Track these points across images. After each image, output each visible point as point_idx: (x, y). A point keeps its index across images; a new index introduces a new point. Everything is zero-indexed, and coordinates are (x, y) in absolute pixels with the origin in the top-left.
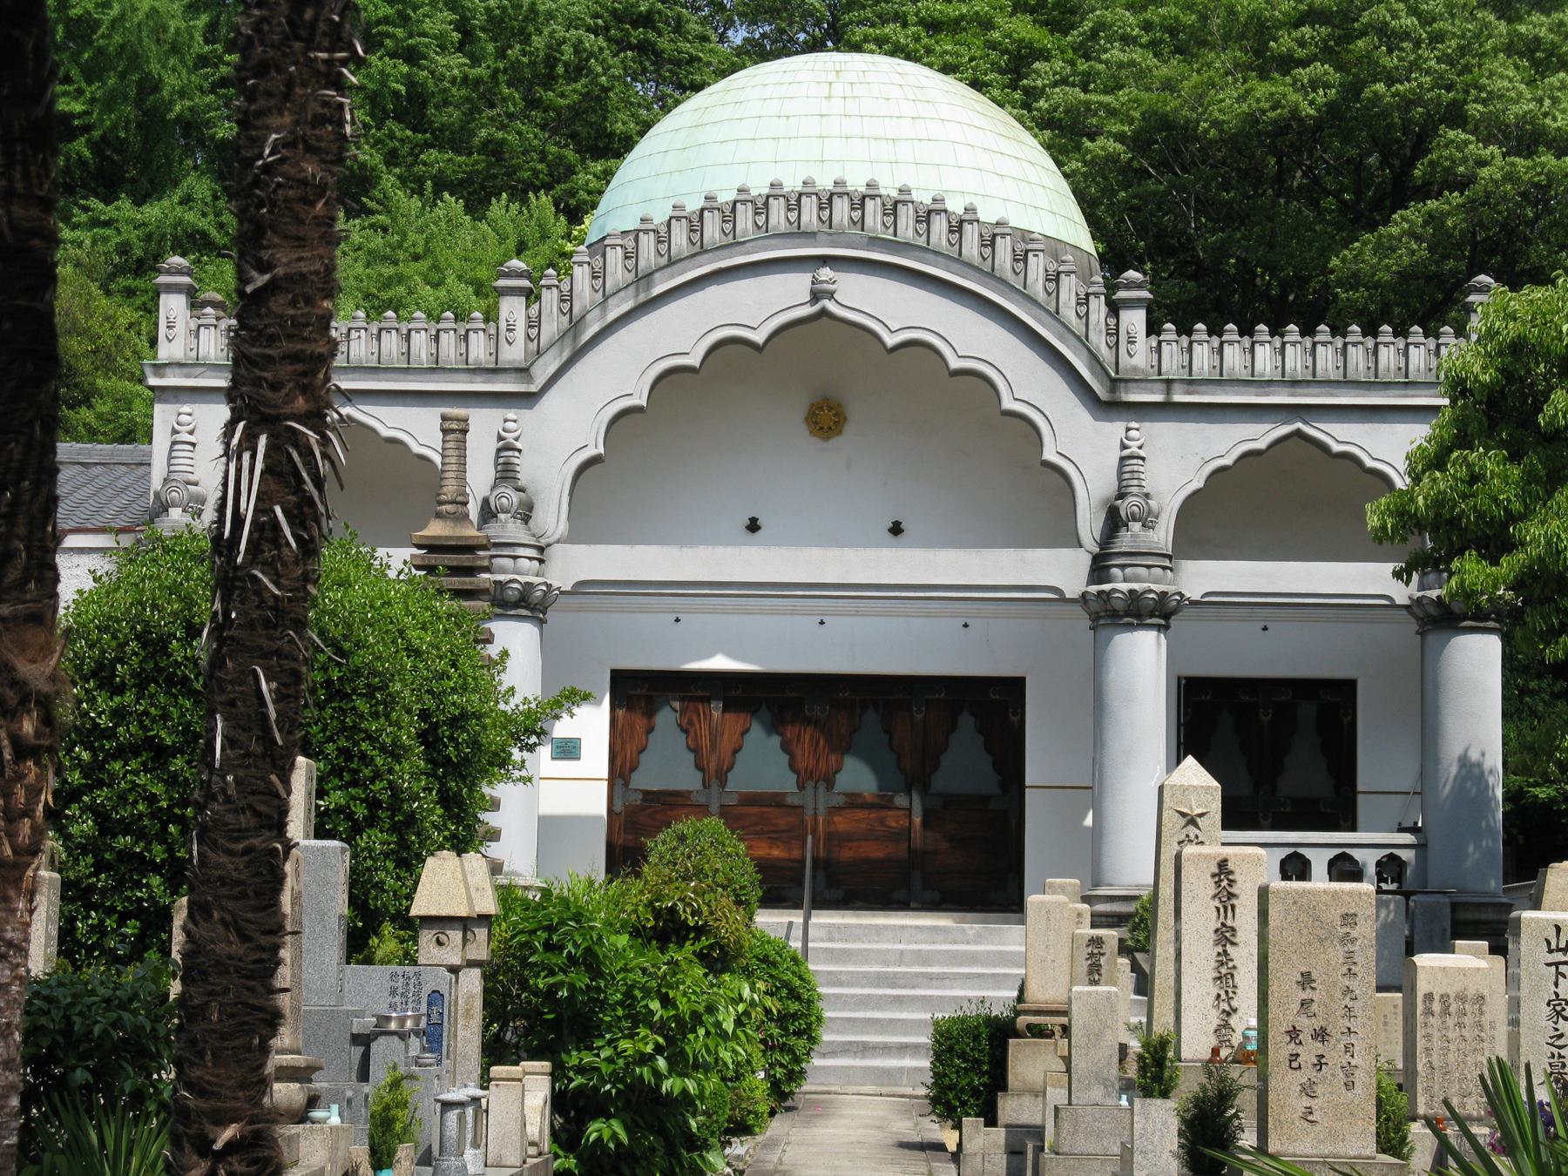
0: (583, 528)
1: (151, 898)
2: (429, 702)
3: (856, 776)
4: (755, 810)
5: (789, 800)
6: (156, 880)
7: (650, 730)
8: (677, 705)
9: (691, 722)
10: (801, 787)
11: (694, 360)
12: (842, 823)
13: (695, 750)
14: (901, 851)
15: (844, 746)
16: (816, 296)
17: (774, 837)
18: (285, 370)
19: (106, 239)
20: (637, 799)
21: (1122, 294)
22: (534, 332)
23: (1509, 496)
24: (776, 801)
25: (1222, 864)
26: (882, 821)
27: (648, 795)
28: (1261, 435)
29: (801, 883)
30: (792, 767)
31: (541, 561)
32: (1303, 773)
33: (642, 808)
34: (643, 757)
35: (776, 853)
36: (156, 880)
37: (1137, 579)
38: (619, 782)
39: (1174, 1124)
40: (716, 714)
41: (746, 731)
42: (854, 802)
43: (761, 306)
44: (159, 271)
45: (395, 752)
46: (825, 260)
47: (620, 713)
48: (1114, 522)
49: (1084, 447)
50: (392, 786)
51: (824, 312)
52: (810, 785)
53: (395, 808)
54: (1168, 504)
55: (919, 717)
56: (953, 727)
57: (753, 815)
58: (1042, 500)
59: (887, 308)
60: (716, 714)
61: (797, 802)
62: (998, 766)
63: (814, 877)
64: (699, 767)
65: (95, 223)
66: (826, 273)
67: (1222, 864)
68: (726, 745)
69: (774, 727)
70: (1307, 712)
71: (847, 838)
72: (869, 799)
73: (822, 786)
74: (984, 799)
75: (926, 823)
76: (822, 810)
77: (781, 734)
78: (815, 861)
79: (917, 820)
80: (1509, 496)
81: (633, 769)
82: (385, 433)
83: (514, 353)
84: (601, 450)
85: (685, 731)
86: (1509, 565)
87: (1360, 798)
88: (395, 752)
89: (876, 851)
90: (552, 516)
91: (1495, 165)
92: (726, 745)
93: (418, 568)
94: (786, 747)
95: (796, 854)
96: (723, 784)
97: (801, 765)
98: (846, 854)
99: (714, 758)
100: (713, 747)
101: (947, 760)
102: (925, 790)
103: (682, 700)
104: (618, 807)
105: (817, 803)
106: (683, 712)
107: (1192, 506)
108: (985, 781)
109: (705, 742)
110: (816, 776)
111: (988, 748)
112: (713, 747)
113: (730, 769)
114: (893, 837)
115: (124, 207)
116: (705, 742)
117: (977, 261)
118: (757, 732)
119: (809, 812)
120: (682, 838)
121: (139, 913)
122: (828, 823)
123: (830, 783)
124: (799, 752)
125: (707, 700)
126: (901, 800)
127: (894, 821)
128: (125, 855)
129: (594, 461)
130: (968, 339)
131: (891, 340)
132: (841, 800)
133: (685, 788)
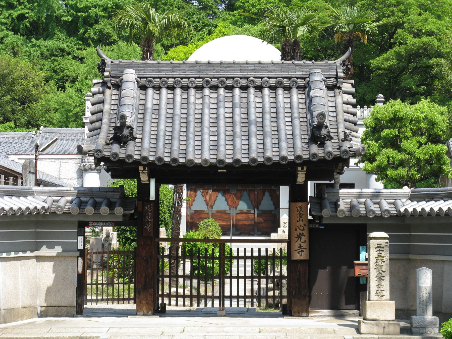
1: (127, 236)
2: (168, 204)
3: (243, 206)
4: (220, 214)
5: (227, 212)
6: (128, 233)
7: (195, 196)
8: (201, 191)
9: (205, 195)
10: (230, 209)
12: (239, 217)
13: (206, 201)
14: (253, 223)
15: (240, 199)
17: (224, 220)
18: (179, 188)
19: (37, 50)
20: (193, 212)
23: (376, 150)
24: (224, 212)
25: (283, 230)
26: (248, 216)
27: (195, 211)
29: (230, 231)
30: (228, 204)
33: (194, 214)
34: (194, 203)
35: (224, 224)
36: (128, 233)
38: (189, 208)
40: (210, 193)
41: (217, 197)
42: (242, 212)
44: (85, 96)
45: (165, 213)
47: (189, 192)
50: (164, 218)
52: (232, 208)
53: (165, 222)
55: (256, 193)
56: (264, 195)
57: (219, 215)
60: (210, 193)
61: (229, 212)
62: (274, 204)
63: (233, 229)
64: (207, 205)
65: (34, 46)
67: (283, 230)
68: (213, 200)
69: (223, 195)
71: (240, 220)
72: (245, 212)
73: (234, 208)
74: (271, 211)
75: (258, 216)
76: (234, 214)
77: (225, 197)
78: (233, 225)
79: (256, 216)
80: (376, 150)
81: (192, 205)
85: (203, 197)
86: (375, 164)
88: (165, 213)
89: (246, 223)
91: (411, 40)
92: (213, 200)
94: (226, 200)
95: (229, 224)
96: (212, 208)
97: (230, 204)
98: (240, 223)
99: (210, 202)
100: (210, 200)
101: (263, 202)
102: (258, 209)
103: (203, 189)
104: (189, 214)
105: (233, 212)
106: (203, 192)
108: (272, 207)
109: (208, 199)
110: (233, 206)
111: (272, 200)
112: (210, 200)
113: (214, 205)
114: (250, 220)
115: (41, 42)
116: (208, 199)
118: (220, 195)
119: (231, 215)
120: (206, 223)
121: (125, 238)
122: (236, 217)
123: (236, 208)
124: (229, 201)
125: (208, 189)
126: (252, 212)
127: (251, 216)
128: (123, 229)
132: (239, 212)
133: (203, 209)
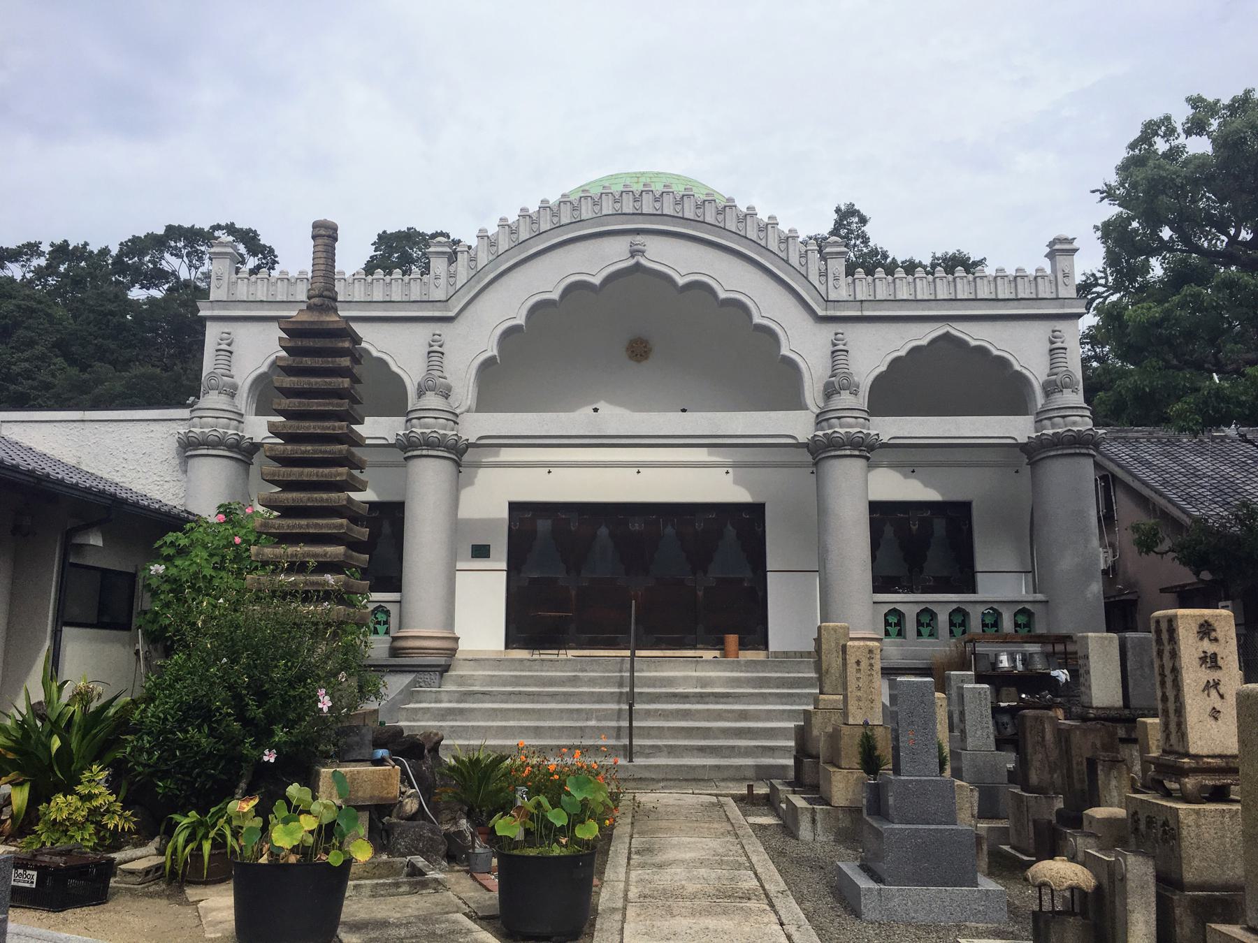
0: (485, 403)
11: (555, 296)
16: (633, 254)
21: (828, 250)
22: (452, 280)
28: (923, 335)
31: (456, 423)
32: (935, 561)
37: (851, 426)
39: (1200, 151)
43: (597, 262)
46: (638, 232)
48: (830, 391)
49: (805, 345)
51: (638, 264)
54: (865, 382)
58: (781, 384)
59: (679, 261)
66: (639, 239)
70: (939, 526)
82: (973, 343)
83: (439, 295)
84: (495, 352)
87: (979, 577)
90: (465, 391)
93: (277, 435)
107: (879, 383)
117: (672, 212)
129: (492, 359)
130: (730, 279)
131: (681, 281)
